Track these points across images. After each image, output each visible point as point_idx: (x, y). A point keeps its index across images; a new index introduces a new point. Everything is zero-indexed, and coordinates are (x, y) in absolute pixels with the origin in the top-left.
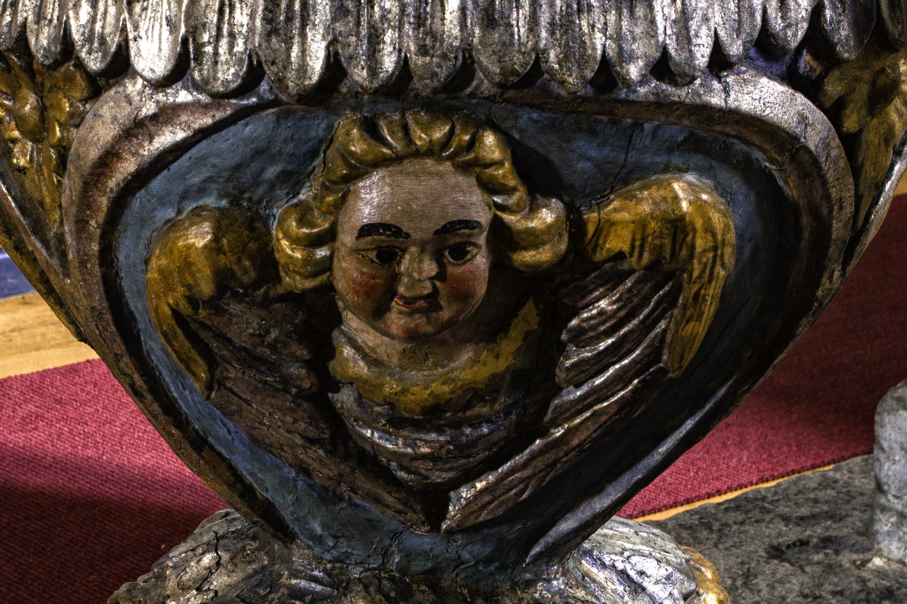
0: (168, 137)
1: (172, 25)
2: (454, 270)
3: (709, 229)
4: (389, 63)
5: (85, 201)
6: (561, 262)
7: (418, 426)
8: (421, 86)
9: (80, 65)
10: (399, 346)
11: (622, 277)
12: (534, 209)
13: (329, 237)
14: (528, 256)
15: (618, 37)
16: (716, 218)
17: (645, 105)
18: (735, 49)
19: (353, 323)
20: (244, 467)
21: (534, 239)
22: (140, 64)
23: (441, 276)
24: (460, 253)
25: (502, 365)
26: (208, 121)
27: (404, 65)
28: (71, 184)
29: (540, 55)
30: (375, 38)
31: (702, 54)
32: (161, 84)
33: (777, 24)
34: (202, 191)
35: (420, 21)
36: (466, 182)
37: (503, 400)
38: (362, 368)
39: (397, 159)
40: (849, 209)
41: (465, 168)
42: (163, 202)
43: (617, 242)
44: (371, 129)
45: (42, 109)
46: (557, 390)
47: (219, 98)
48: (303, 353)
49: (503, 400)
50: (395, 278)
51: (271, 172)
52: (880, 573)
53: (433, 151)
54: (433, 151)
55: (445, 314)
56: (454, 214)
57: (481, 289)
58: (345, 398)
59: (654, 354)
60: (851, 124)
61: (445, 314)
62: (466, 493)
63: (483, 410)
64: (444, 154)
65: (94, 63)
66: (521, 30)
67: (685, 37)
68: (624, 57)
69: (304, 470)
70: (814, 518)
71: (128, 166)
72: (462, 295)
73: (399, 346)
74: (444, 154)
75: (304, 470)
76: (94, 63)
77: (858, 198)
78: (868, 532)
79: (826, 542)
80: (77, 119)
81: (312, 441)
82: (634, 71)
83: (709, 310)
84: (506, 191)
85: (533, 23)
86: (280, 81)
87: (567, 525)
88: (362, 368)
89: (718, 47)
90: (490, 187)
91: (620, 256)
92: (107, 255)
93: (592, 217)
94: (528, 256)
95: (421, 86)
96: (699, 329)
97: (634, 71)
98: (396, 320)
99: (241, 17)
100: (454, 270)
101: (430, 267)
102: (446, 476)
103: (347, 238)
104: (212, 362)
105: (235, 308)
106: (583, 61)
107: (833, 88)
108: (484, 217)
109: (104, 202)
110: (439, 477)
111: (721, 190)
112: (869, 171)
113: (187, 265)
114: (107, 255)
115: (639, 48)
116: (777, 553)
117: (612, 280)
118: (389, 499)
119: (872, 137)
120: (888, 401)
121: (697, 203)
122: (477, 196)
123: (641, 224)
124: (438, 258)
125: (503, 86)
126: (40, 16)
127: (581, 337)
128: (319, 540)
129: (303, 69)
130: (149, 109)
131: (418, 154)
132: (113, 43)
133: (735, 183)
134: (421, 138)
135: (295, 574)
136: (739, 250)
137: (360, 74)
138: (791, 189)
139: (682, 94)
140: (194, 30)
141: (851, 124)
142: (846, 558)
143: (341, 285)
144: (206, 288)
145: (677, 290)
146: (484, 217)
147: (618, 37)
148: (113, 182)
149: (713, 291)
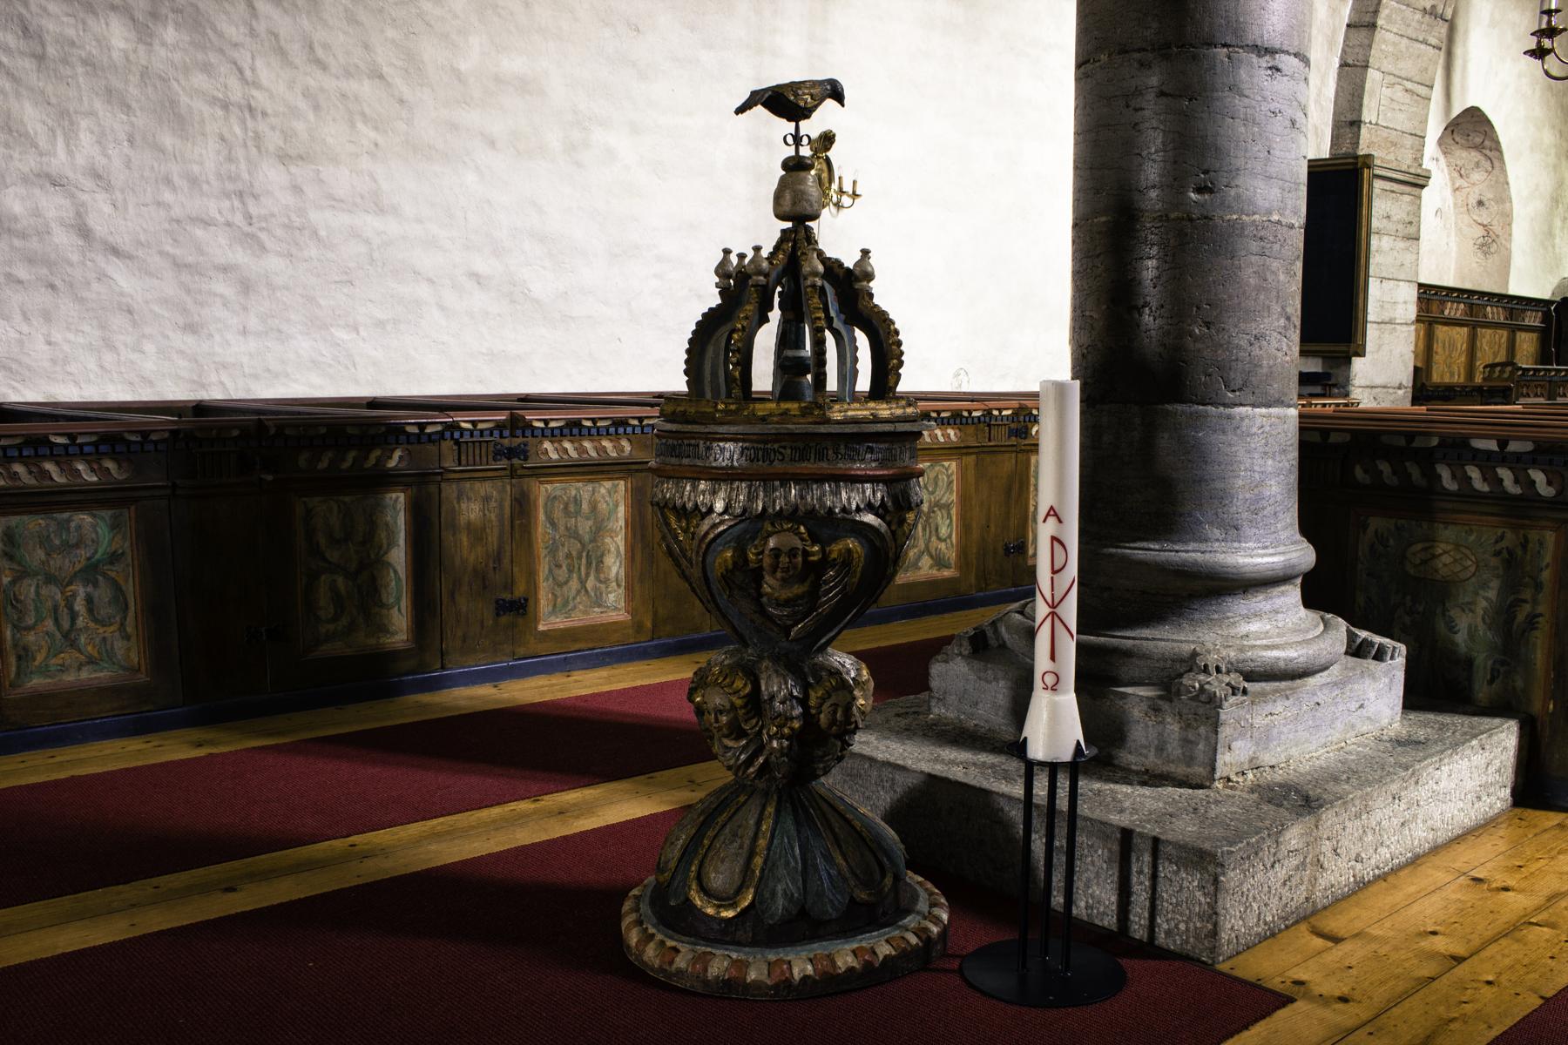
0: (721, 528)
1: (724, 500)
2: (793, 560)
3: (857, 552)
4: (778, 508)
5: (699, 546)
6: (820, 560)
7: (783, 606)
8: (785, 513)
9: (700, 511)
10: (779, 583)
11: (835, 565)
12: (813, 546)
13: (762, 553)
14: (812, 558)
15: (833, 502)
16: (859, 550)
17: (839, 519)
18: (862, 506)
19: (767, 578)
20: (736, 623)
21: (813, 554)
22: (716, 510)
23: (790, 562)
24: (795, 556)
25: (805, 589)
26: (732, 523)
27: (781, 508)
28: (696, 542)
29: (814, 506)
30: (774, 502)
31: (854, 507)
32: (721, 514)
33: (873, 501)
34: (730, 542)
35: (785, 498)
36: (797, 538)
37: (805, 600)
38: (769, 590)
39: (779, 532)
40: (894, 550)
41: (796, 534)
42: (720, 545)
43: (834, 555)
44: (773, 525)
45: (688, 524)
46: (820, 598)
47: (736, 517)
48: (754, 586)
49: (805, 600)
50: (778, 563)
51: (748, 536)
52: (932, 719)
53: (788, 530)
54: (788, 530)
55: (791, 573)
56: (794, 546)
57: (800, 566)
58: (764, 600)
59: (844, 588)
60: (893, 528)
61: (791, 573)
62: (796, 629)
63: (800, 602)
64: (779, 289)
65: (704, 510)
66: (809, 499)
67: (850, 503)
68: (835, 507)
69: (752, 621)
70: (911, 707)
71: (711, 536)
72: (795, 567)
73: (779, 583)
74: (779, 289)
75: (752, 621)
76: (704, 510)
77: (896, 548)
78: (929, 709)
79: (915, 713)
80: (698, 525)
81: (755, 612)
82: (837, 510)
83: (858, 575)
84: (806, 541)
85: (812, 499)
86: (751, 512)
87: (823, 641)
88: (769, 590)
89: (858, 506)
90: (803, 540)
91: (835, 559)
92: (704, 561)
93: (828, 549)
94: (812, 558)
95: (785, 513)
96: (855, 580)
97: (837, 510)
98: (779, 575)
99: (741, 497)
100: (793, 560)
101: (787, 560)
102: (791, 622)
103: (767, 552)
104: (730, 588)
105: (737, 573)
106: (824, 508)
107: (888, 518)
108: (801, 547)
109: (704, 546)
110: (789, 622)
111: (859, 542)
112: (899, 542)
113: (726, 561)
114: (704, 561)
115: (838, 505)
116: (898, 715)
117: (833, 567)
118: (775, 629)
119: (899, 532)
120: (933, 660)
121: (854, 546)
122: (799, 541)
123: (840, 550)
124: (789, 557)
125: (805, 513)
126: (689, 499)
127: (826, 583)
128: (755, 644)
129: (757, 509)
130: (718, 521)
131: (785, 530)
132: (709, 504)
133: (864, 541)
134: (785, 527)
135: (749, 656)
136: (865, 560)
137: (771, 510)
138: (878, 543)
139: (849, 516)
140: (730, 501)
141: (893, 528)
142: (921, 717)
143: (765, 565)
144: (730, 567)
145: (849, 570)
146: (801, 547)
147: (833, 502)
148: (707, 541)
149: (859, 569)
